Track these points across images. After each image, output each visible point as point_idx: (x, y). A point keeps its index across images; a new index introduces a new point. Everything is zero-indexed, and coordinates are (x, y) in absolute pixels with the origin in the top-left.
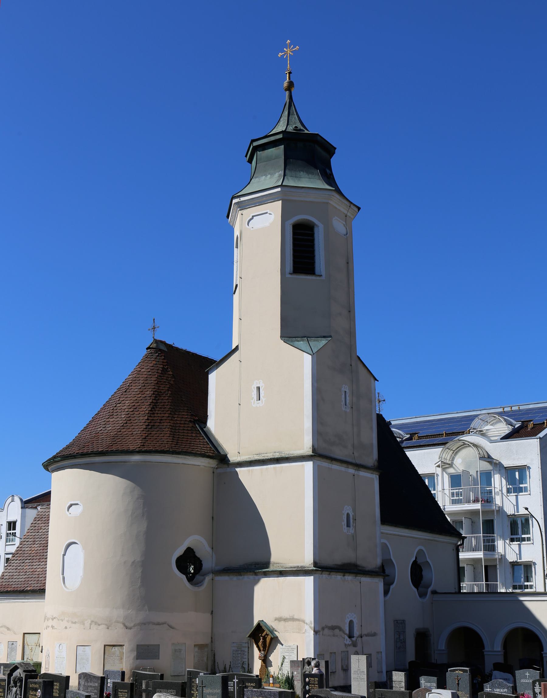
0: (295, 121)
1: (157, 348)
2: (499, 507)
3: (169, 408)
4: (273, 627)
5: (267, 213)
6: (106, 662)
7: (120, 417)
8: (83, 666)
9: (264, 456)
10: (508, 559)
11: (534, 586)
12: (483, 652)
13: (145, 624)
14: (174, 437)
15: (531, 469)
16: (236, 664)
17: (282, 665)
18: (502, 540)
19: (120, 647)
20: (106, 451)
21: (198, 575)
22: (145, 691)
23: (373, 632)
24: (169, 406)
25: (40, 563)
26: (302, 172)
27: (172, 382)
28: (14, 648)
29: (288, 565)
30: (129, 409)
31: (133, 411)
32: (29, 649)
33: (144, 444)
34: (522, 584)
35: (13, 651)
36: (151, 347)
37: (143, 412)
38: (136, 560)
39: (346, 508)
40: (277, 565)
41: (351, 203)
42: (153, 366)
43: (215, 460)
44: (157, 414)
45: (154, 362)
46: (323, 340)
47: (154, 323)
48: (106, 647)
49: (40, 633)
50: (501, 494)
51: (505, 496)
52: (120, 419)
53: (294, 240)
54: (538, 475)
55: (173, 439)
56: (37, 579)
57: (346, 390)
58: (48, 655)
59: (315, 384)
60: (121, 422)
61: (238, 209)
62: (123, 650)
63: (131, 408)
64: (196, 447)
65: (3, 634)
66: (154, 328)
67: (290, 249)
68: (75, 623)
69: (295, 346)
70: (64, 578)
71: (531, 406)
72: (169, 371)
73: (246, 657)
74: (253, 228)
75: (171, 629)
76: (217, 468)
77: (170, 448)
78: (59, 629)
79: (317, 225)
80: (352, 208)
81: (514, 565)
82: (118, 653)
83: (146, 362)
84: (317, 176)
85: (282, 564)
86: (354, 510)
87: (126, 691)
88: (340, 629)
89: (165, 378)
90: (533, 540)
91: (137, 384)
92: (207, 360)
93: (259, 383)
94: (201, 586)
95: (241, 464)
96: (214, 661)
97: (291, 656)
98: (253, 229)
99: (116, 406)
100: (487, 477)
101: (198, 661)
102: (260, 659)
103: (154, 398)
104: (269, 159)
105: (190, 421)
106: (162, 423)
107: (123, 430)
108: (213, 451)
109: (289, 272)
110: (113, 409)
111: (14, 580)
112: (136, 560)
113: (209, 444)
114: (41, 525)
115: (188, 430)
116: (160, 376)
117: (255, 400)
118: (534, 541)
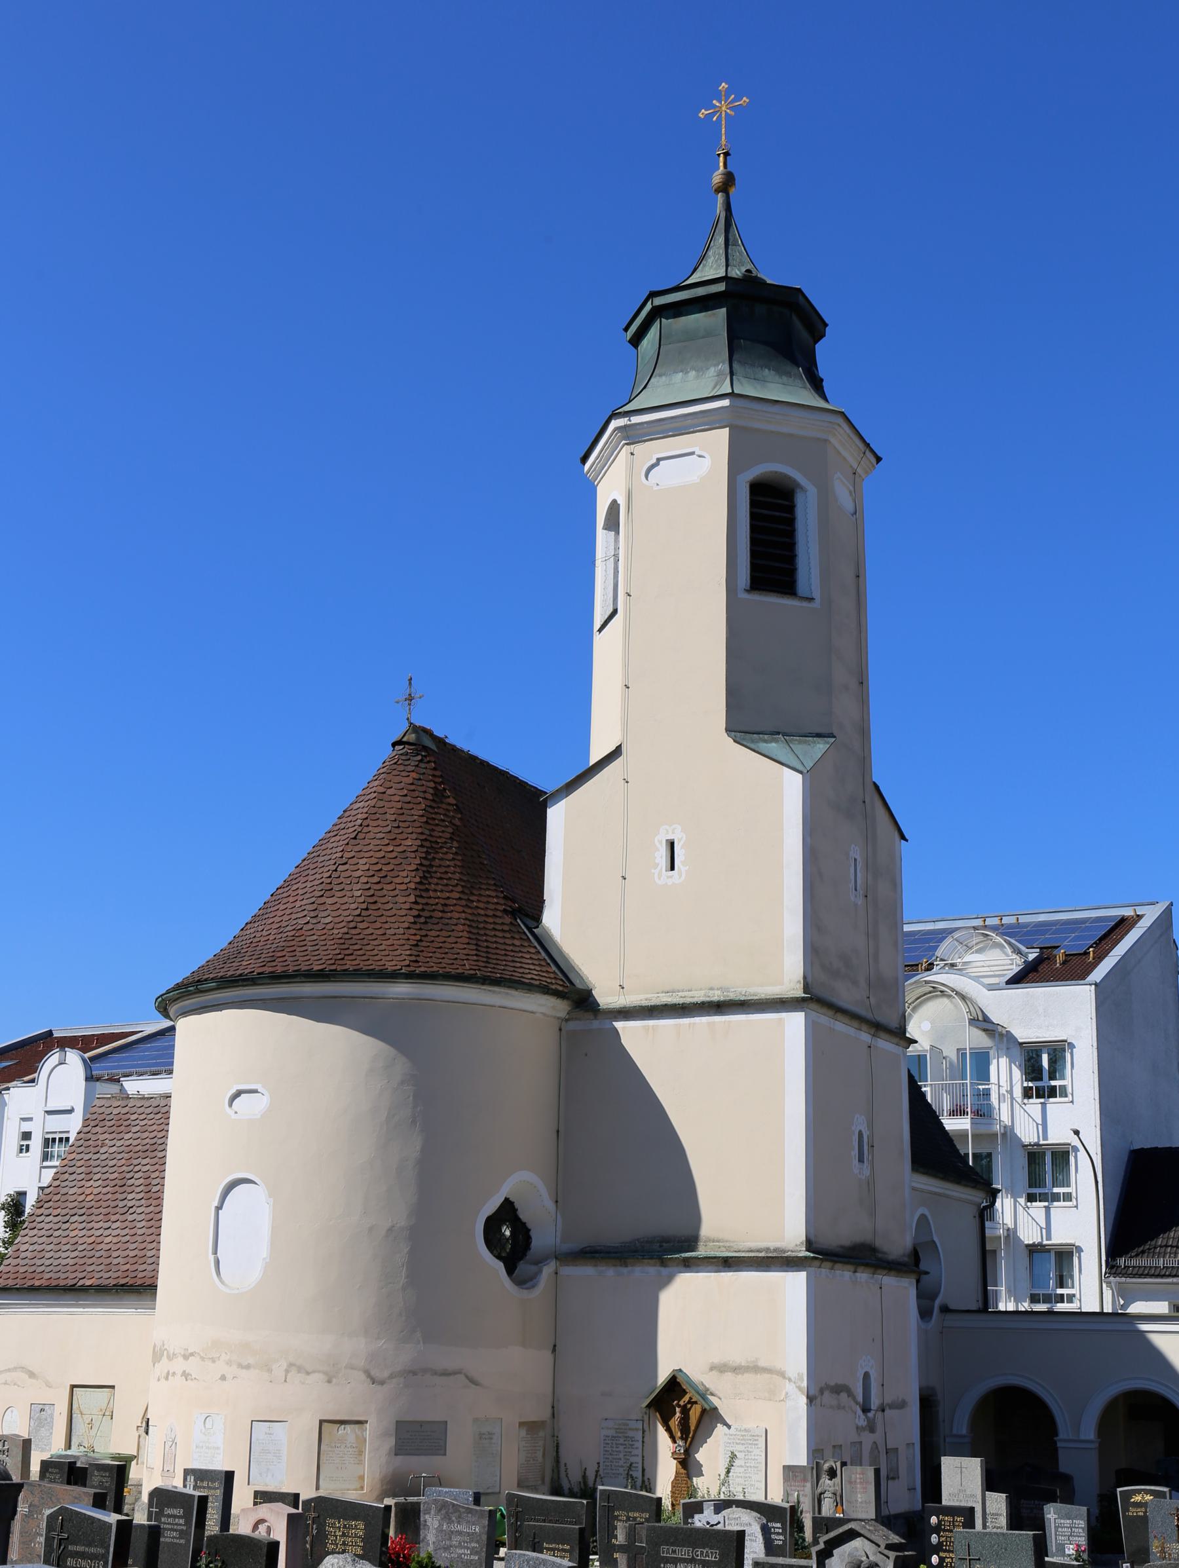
0: (741, 259)
1: (419, 743)
2: (1005, 1127)
3: (458, 878)
4: (705, 1387)
5: (692, 453)
6: (325, 1461)
7: (350, 894)
8: (268, 1469)
9: (685, 997)
10: (1022, 1237)
11: (1078, 1296)
12: (1055, 1443)
13: (415, 1373)
14: (480, 946)
15: (1075, 1048)
16: (613, 1467)
17: (728, 1472)
18: (1011, 1198)
19: (357, 1426)
20: (331, 971)
21: (522, 1262)
22: (622, 1549)
23: (900, 1399)
24: (457, 874)
25: (109, 1224)
26: (767, 370)
27: (457, 822)
28: (46, 1420)
29: (743, 1244)
30: (370, 878)
31: (379, 882)
32: (84, 1423)
33: (418, 959)
34: (1050, 1292)
35: (43, 1427)
36: (405, 739)
37: (404, 887)
38: (397, 1224)
39: (857, 1118)
40: (714, 1244)
41: (868, 445)
42: (412, 784)
43: (565, 1002)
44: (435, 891)
45: (414, 775)
46: (818, 743)
47: (410, 688)
48: (325, 1425)
49: (113, 1387)
50: (1009, 1100)
51: (1019, 1104)
52: (351, 900)
53: (753, 516)
54: (1091, 1061)
55: (477, 950)
56: (108, 1261)
57: (856, 857)
58: (173, 1441)
59: (809, 840)
60: (353, 906)
61: (624, 442)
62: (364, 1433)
63: (373, 875)
64: (528, 971)
65: (19, 1386)
66: (410, 698)
68: (248, 1367)
69: (763, 752)
70: (217, 1262)
71: (1042, 918)
72: (449, 797)
73: (639, 1452)
74: (658, 485)
75: (473, 1386)
76: (567, 1020)
77: (475, 970)
78: (204, 1381)
79: (802, 488)
80: (868, 456)
81: (1034, 1250)
82: (351, 1439)
83: (395, 773)
84: (799, 381)
85: (727, 1241)
86: (871, 1125)
87: (567, 1547)
88: (850, 1394)
89: (441, 811)
90: (1077, 1199)
91: (380, 822)
92: (507, 777)
93: (673, 833)
94: (533, 1287)
95: (627, 1013)
96: (557, 1460)
98: (658, 488)
99: (336, 870)
100: (981, 1062)
101: (526, 1461)
102: (674, 1459)
103: (424, 855)
104: (690, 336)
105: (505, 911)
106: (447, 912)
107: (361, 926)
108: (561, 980)
109: (744, 587)
110: (330, 877)
111: (48, 1262)
112: (397, 1224)
113: (549, 964)
114: (102, 1137)
115: (503, 931)
116: (430, 807)
118: (1079, 1201)
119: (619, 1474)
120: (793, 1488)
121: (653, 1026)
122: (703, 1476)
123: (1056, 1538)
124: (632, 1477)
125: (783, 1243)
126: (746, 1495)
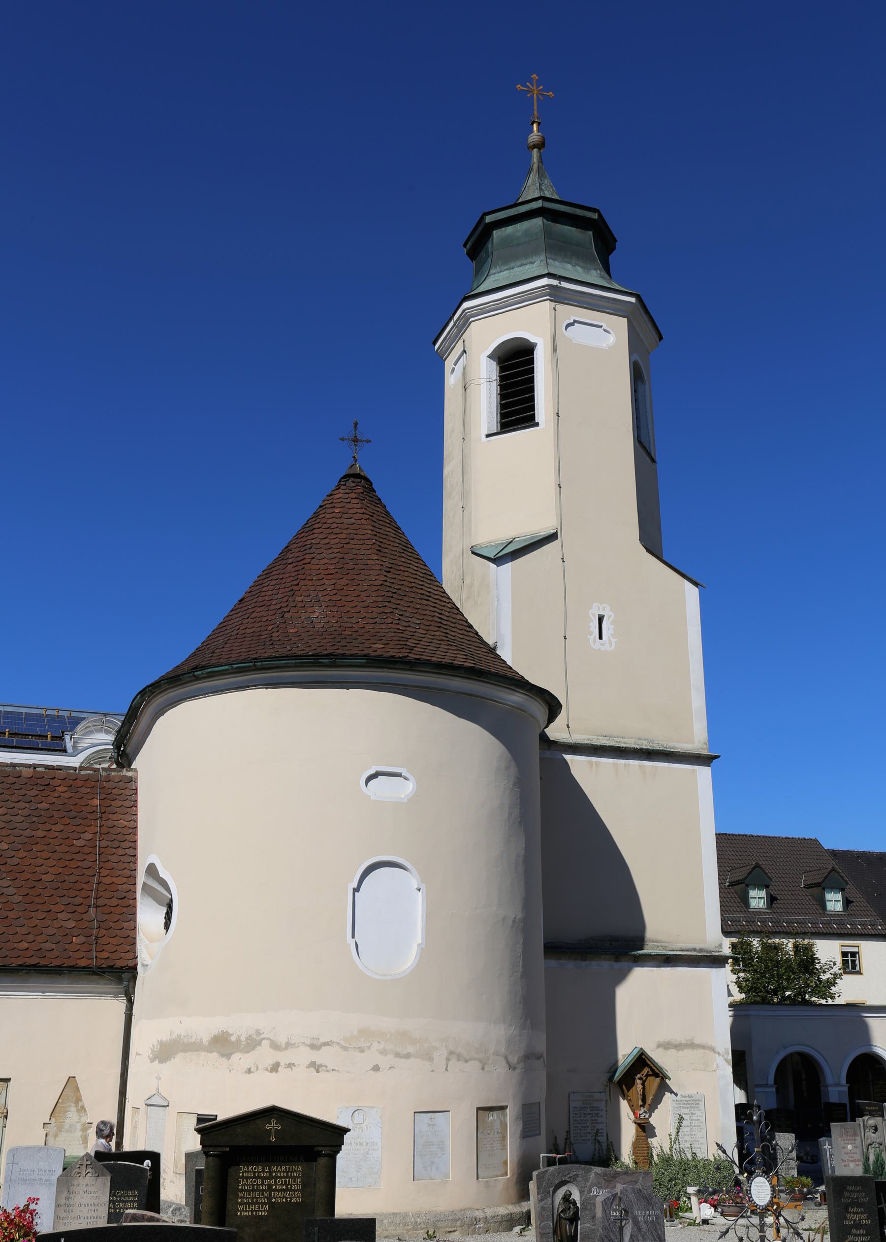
5: (601, 327)
40: (654, 944)
47: (355, 430)
67: (538, 399)
68: (408, 1056)
85: (663, 942)
93: (604, 610)
97: (694, 1114)
117: (595, 637)
119: (587, 1140)
120: (846, 1142)
121: (596, 762)
122: (656, 1136)
123: (831, 1163)
124: (599, 1142)
125: (706, 945)
126: (693, 1149)
